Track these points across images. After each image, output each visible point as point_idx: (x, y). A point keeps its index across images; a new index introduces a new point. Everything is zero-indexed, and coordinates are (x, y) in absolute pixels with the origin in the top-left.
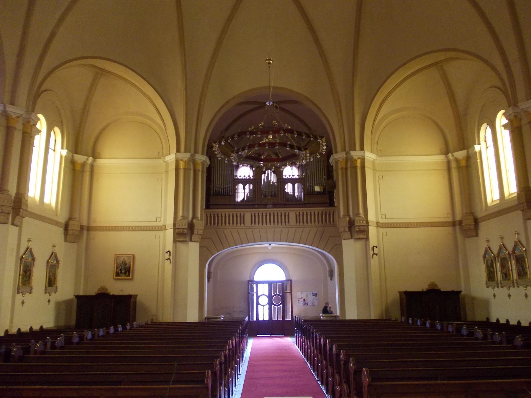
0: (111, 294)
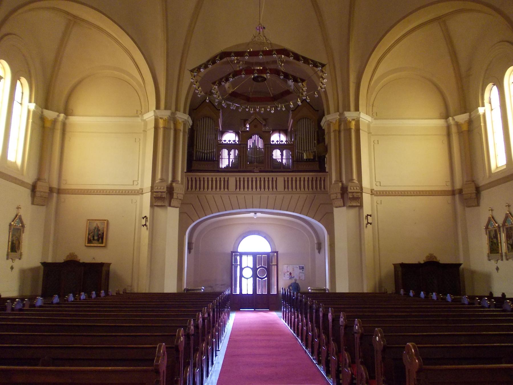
0: (81, 261)
